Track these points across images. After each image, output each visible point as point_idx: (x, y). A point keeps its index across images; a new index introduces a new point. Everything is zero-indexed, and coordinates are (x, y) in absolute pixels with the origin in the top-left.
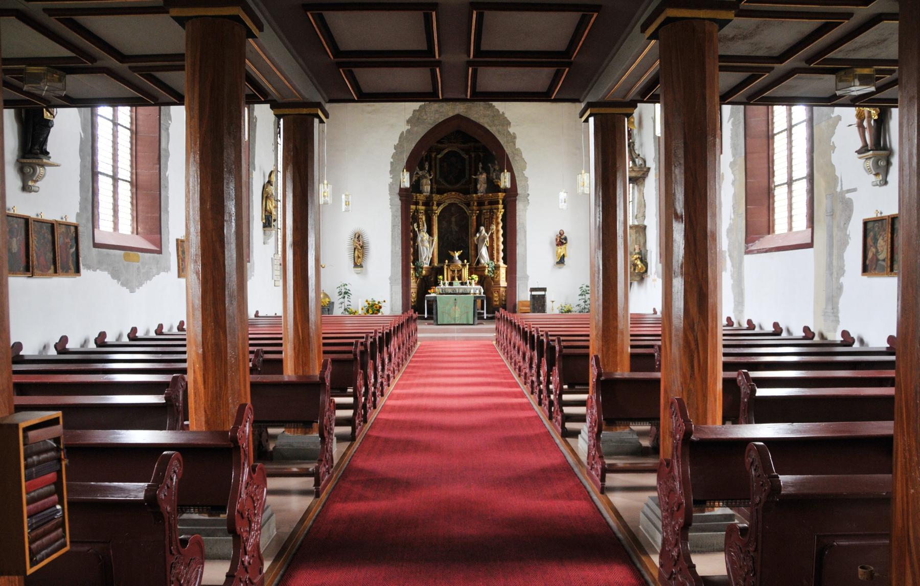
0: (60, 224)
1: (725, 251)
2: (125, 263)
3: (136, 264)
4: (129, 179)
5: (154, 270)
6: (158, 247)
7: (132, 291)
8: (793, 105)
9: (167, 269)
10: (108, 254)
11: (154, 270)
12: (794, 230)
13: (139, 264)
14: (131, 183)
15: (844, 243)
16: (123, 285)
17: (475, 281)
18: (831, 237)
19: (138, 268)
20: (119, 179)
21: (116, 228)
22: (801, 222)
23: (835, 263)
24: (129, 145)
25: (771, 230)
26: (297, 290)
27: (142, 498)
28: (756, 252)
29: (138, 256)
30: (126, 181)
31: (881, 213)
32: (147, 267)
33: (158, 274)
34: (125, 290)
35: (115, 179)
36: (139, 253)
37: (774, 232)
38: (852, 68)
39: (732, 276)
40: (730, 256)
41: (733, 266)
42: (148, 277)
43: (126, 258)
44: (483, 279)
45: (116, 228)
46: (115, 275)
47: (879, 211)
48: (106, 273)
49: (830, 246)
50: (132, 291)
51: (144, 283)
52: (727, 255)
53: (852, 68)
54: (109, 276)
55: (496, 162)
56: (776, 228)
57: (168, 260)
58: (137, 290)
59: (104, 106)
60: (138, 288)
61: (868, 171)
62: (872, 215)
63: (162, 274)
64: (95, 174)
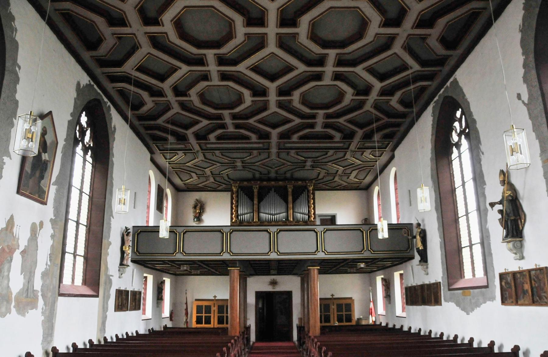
0: (533, 270)
2: (463, 297)
4: (86, 224)
5: (481, 301)
6: (96, 293)
8: (477, 211)
9: (493, 299)
10: (454, 293)
11: (481, 301)
12: (476, 276)
13: (470, 297)
14: (86, 226)
16: (462, 310)
19: (470, 300)
20: (69, 219)
21: (474, 275)
22: (480, 273)
24: (90, 178)
25: (463, 276)
29: (470, 292)
30: (84, 225)
31: (508, 270)
32: (476, 298)
33: (485, 302)
35: (78, 223)
36: (471, 290)
37: (464, 277)
40: (42, 295)
42: (478, 305)
43: (464, 294)
45: (474, 275)
46: (458, 304)
47: (521, 267)
50: (468, 314)
52: (40, 294)
54: (455, 305)
55: (383, 233)
56: (465, 275)
58: (471, 313)
59: (468, 144)
61: (510, 250)
62: (503, 271)
63: (488, 303)
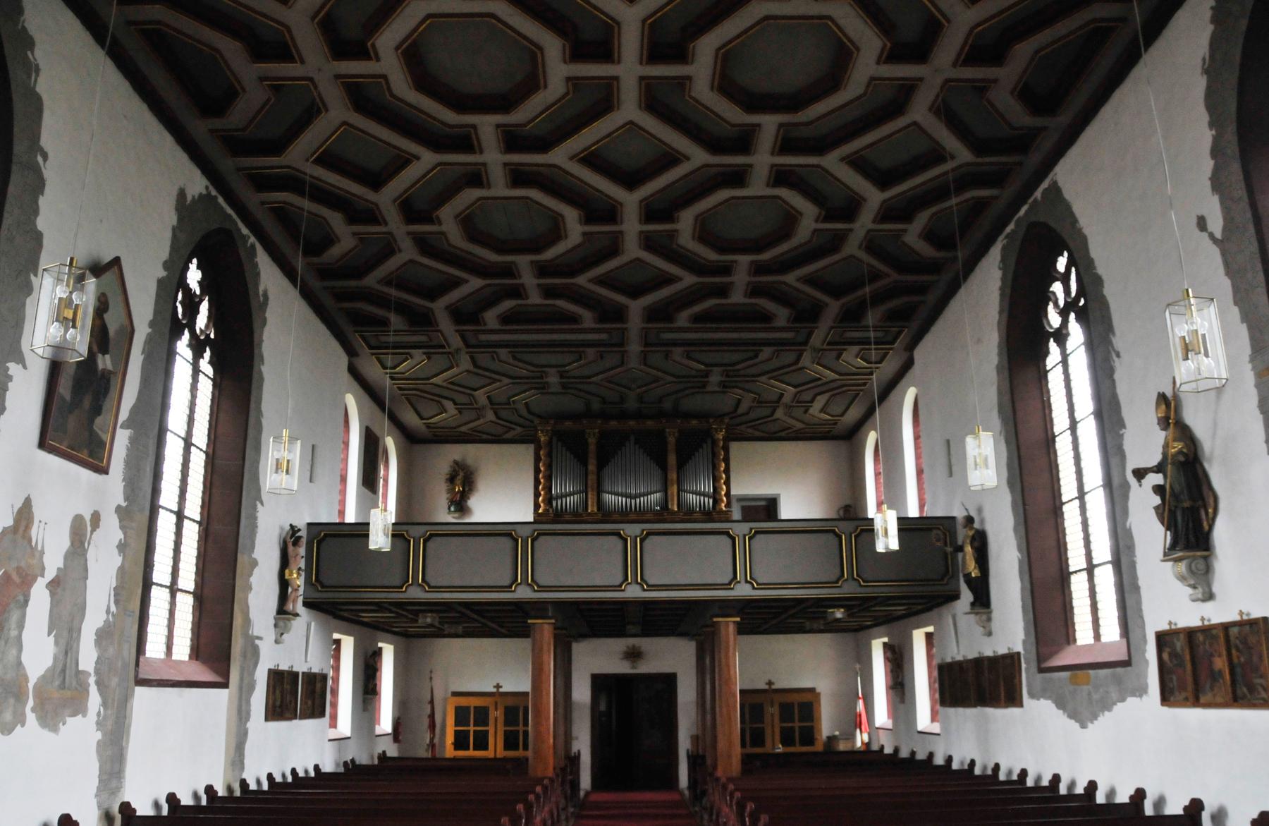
1: (87, 674)
2: (1071, 688)
3: (1085, 688)
5: (1114, 695)
7: (1083, 726)
9: (1141, 691)
11: (1114, 695)
13: (1090, 687)
15: (252, 687)
16: (1071, 716)
17: (1056, 305)
18: (242, 679)
19: (1089, 694)
21: (1097, 636)
23: (244, 708)
26: (274, 692)
27: (389, 550)
28: (155, 683)
29: (1088, 676)
32: (1101, 690)
33: (1123, 700)
34: (1074, 725)
38: (727, 804)
39: (100, 725)
40: (98, 683)
41: (105, 704)
42: (1107, 706)
43: (1074, 681)
44: (1192, 539)
45: (1097, 636)
46: (1061, 704)
48: (1050, 702)
49: (241, 688)
51: (1099, 716)
52: (92, 680)
53: (727, 804)
57: (1143, 676)
60: (1092, 723)
63: (1131, 701)
64: (1117, 563)
